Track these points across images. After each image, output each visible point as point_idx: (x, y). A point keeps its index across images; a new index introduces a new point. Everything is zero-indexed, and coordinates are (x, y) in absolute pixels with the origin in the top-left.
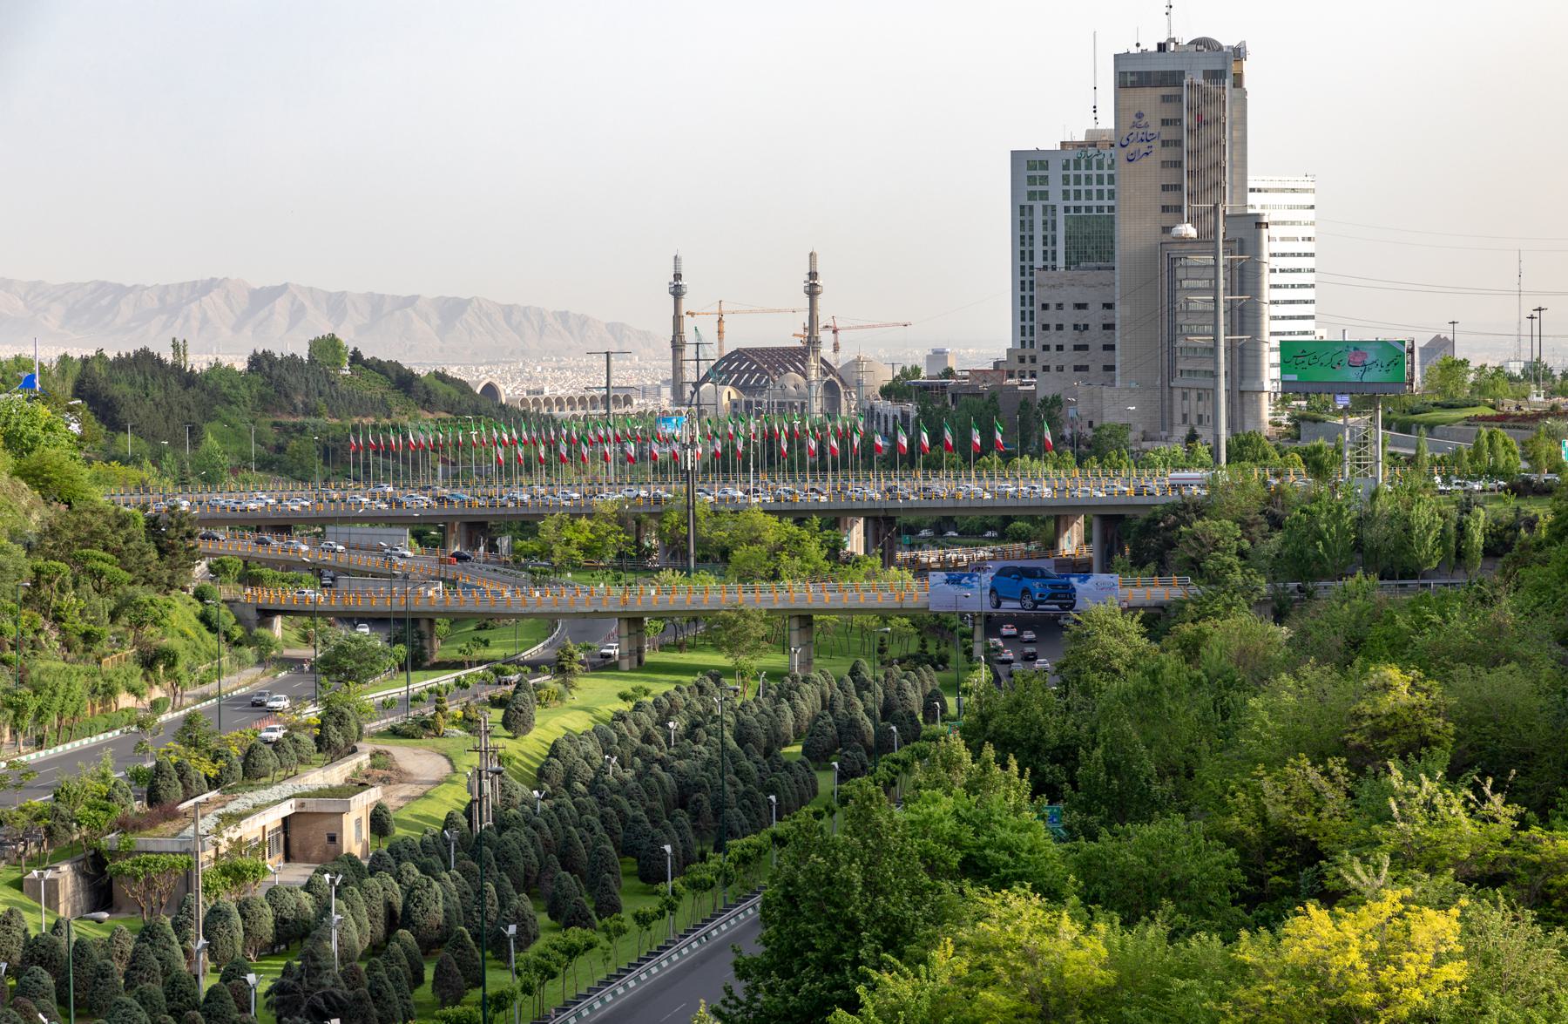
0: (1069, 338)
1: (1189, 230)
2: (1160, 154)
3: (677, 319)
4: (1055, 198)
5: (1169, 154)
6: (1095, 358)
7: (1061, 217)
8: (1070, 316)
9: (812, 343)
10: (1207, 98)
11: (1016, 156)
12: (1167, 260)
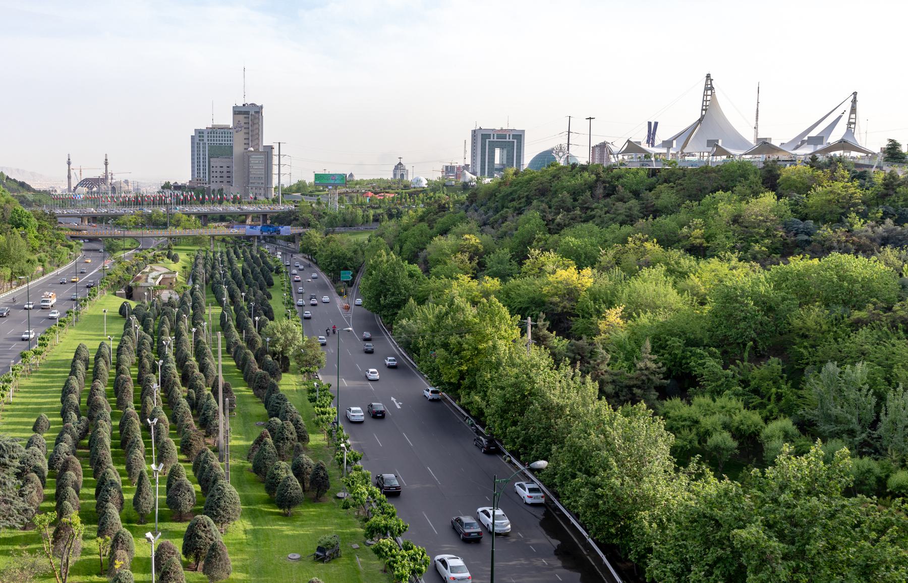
0: (218, 175)
1: (252, 149)
2: (244, 131)
3: (69, 170)
4: (206, 141)
5: (246, 131)
8: (219, 169)
10: (255, 118)
12: (246, 157)
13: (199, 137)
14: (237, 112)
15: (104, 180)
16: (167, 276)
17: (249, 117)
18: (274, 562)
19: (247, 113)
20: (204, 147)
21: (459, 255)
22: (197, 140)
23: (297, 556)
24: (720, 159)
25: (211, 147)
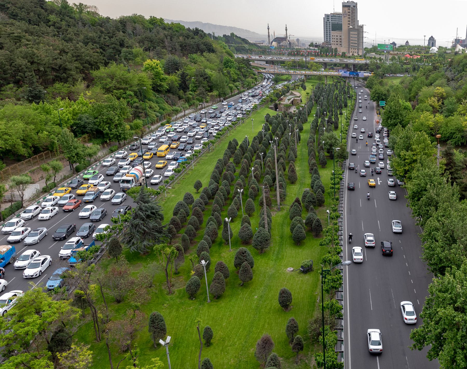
0: (336, 40)
3: (269, 32)
4: (330, 21)
6: (339, 43)
8: (336, 37)
9: (287, 37)
15: (285, 39)
16: (296, 98)
18: (280, 272)
19: (349, 6)
21: (433, 98)
22: (326, 19)
23: (292, 269)
24: (55, 273)
25: (333, 24)
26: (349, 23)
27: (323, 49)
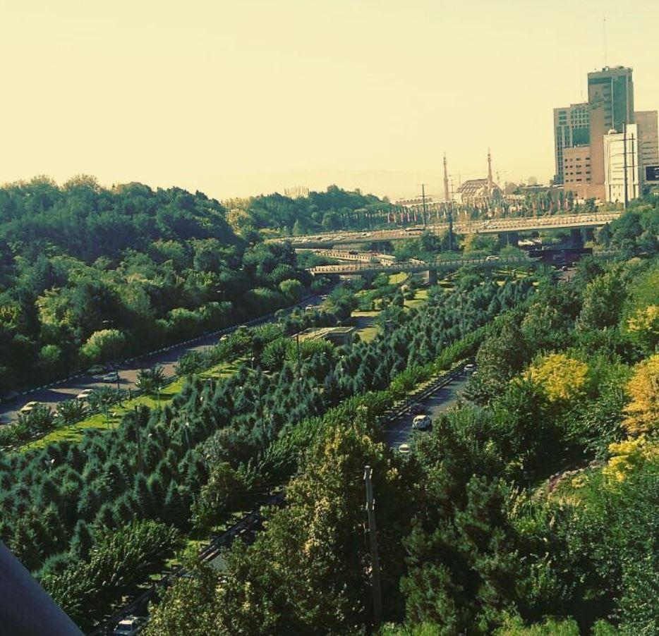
0: (575, 170)
7: (571, 129)
8: (575, 163)
9: (490, 177)
11: (555, 110)
13: (560, 115)
14: (594, 80)
17: (197, 191)
19: (607, 80)
20: (567, 133)
26: (608, 121)
27: (166, 193)
